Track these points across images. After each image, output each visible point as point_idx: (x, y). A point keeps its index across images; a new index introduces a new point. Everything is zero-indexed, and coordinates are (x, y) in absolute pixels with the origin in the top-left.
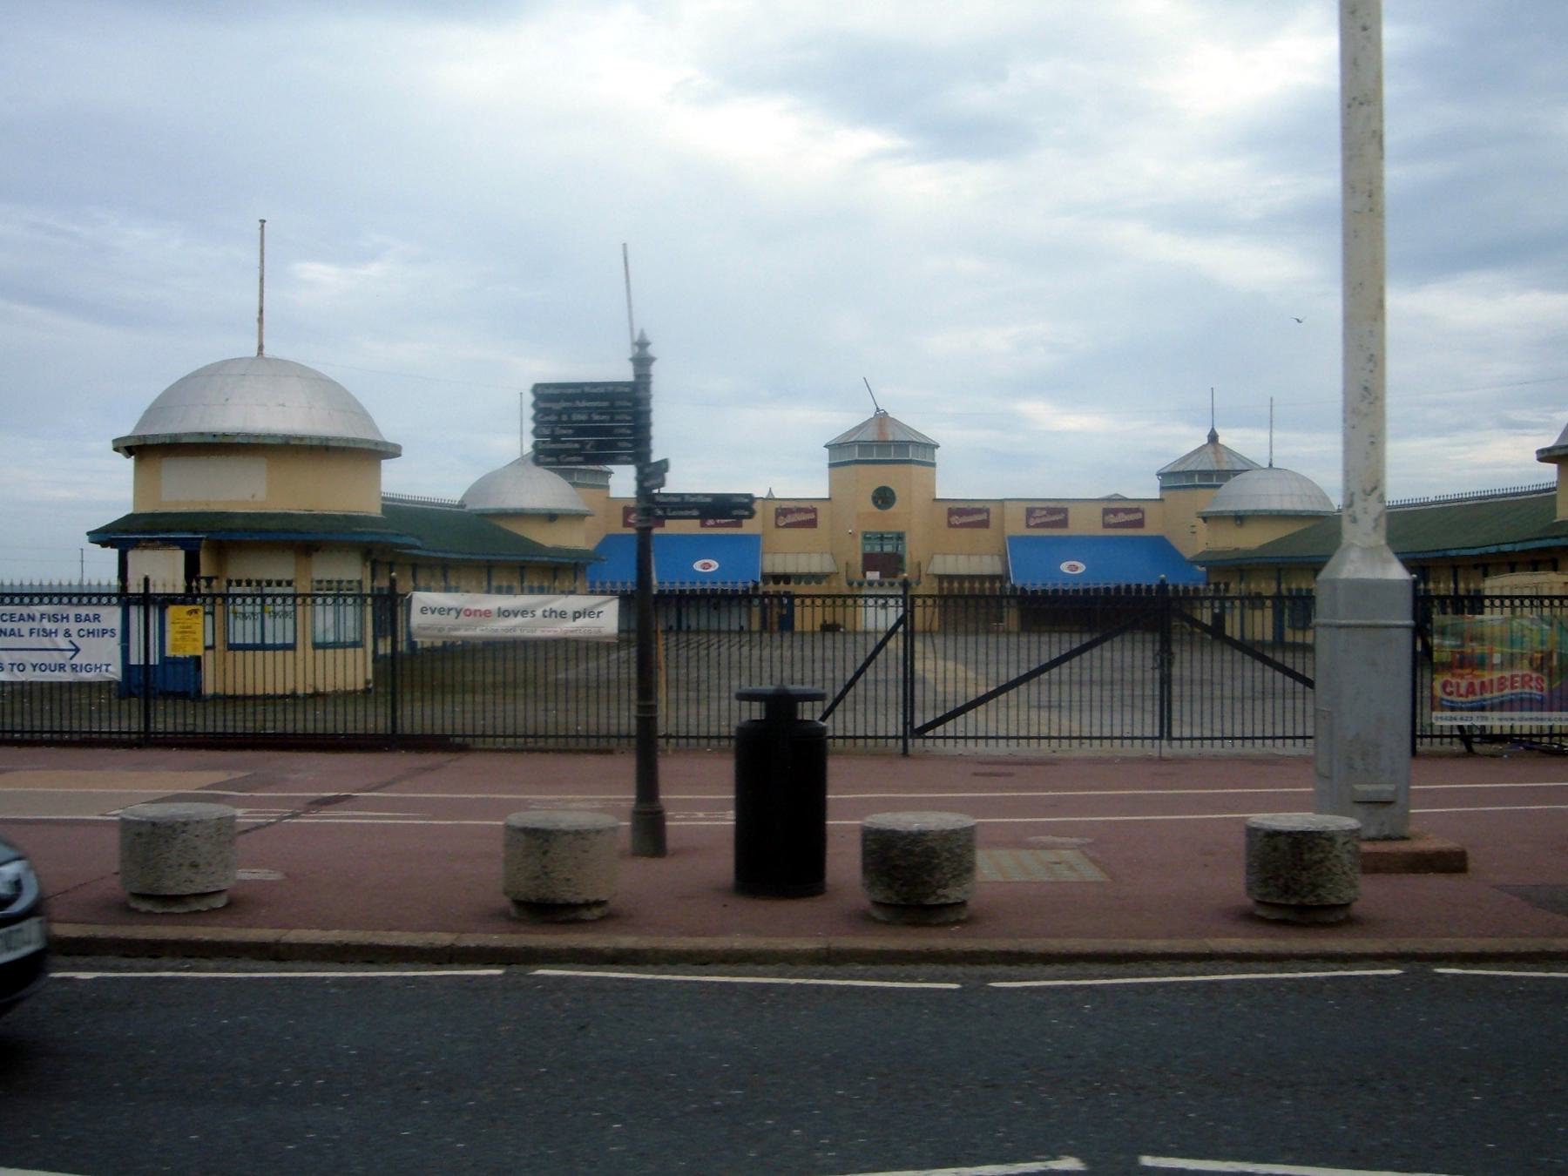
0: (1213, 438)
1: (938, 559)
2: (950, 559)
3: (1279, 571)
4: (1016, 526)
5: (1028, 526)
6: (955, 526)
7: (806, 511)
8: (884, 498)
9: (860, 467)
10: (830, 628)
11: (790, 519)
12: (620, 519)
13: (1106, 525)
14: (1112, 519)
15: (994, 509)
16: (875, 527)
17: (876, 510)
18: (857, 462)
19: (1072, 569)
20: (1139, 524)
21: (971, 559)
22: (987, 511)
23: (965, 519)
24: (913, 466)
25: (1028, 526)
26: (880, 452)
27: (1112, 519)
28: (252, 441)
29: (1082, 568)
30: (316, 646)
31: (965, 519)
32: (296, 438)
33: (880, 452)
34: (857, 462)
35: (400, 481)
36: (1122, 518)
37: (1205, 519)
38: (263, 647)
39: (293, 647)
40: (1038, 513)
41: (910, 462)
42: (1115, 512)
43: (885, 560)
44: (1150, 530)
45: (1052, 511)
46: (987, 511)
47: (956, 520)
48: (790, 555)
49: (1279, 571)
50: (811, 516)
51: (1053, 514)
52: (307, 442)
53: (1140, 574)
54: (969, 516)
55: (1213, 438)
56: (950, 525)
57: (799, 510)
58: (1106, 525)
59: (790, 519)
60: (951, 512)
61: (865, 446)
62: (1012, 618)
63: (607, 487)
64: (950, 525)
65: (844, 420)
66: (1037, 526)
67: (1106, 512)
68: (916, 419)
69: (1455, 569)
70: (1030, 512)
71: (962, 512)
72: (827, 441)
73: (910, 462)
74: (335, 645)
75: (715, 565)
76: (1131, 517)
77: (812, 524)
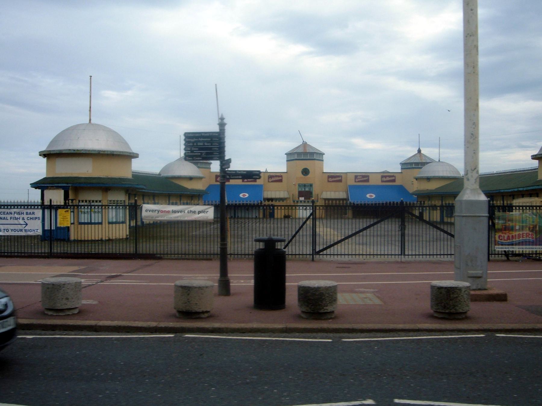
0: (419, 151)
1: (324, 193)
2: (329, 193)
3: (442, 197)
4: (351, 182)
5: (355, 182)
6: (330, 182)
7: (279, 176)
8: (305, 172)
9: (297, 161)
10: (287, 217)
11: (273, 179)
12: (214, 179)
13: (382, 181)
14: (384, 179)
15: (343, 176)
16: (303, 182)
17: (303, 176)
18: (296, 159)
19: (371, 196)
20: (394, 181)
21: (336, 193)
22: (341, 176)
23: (334, 179)
24: (316, 161)
25: (355, 182)
26: (304, 156)
27: (384, 179)
28: (87, 152)
29: (374, 196)
30: (109, 223)
31: (334, 179)
32: (102, 151)
33: (304, 156)
34: (296, 159)
35: (138, 166)
36: (388, 179)
37: (416, 179)
38: (91, 223)
39: (101, 223)
40: (359, 177)
41: (314, 159)
42: (386, 177)
43: (306, 193)
44: (397, 183)
45: (363, 177)
46: (341, 176)
47: (330, 179)
48: (273, 192)
49: (442, 197)
50: (280, 178)
51: (364, 177)
52: (106, 153)
53: (394, 198)
54: (335, 178)
55: (419, 151)
56: (328, 181)
57: (276, 176)
58: (382, 181)
59: (273, 179)
60: (329, 177)
61: (299, 154)
62: (350, 213)
63: (210, 168)
64: (328, 181)
65: (292, 145)
66: (359, 182)
67: (382, 177)
68: (317, 145)
69: (503, 196)
70: (356, 177)
71: (332, 177)
72: (286, 152)
73: (314, 159)
74: (116, 223)
75: (247, 195)
76: (391, 179)
77: (281, 181)
